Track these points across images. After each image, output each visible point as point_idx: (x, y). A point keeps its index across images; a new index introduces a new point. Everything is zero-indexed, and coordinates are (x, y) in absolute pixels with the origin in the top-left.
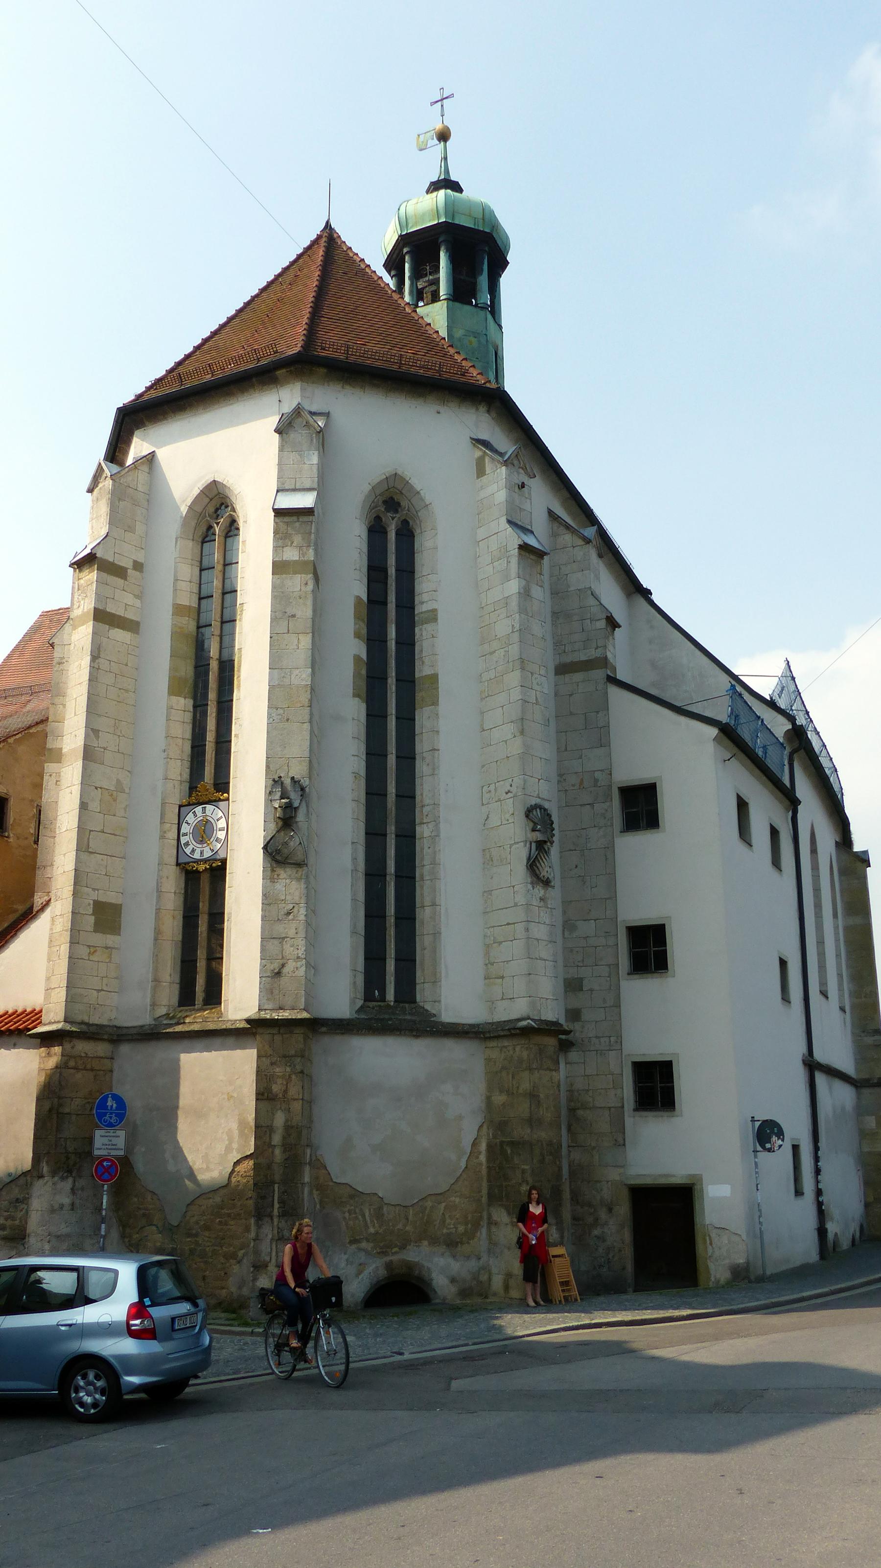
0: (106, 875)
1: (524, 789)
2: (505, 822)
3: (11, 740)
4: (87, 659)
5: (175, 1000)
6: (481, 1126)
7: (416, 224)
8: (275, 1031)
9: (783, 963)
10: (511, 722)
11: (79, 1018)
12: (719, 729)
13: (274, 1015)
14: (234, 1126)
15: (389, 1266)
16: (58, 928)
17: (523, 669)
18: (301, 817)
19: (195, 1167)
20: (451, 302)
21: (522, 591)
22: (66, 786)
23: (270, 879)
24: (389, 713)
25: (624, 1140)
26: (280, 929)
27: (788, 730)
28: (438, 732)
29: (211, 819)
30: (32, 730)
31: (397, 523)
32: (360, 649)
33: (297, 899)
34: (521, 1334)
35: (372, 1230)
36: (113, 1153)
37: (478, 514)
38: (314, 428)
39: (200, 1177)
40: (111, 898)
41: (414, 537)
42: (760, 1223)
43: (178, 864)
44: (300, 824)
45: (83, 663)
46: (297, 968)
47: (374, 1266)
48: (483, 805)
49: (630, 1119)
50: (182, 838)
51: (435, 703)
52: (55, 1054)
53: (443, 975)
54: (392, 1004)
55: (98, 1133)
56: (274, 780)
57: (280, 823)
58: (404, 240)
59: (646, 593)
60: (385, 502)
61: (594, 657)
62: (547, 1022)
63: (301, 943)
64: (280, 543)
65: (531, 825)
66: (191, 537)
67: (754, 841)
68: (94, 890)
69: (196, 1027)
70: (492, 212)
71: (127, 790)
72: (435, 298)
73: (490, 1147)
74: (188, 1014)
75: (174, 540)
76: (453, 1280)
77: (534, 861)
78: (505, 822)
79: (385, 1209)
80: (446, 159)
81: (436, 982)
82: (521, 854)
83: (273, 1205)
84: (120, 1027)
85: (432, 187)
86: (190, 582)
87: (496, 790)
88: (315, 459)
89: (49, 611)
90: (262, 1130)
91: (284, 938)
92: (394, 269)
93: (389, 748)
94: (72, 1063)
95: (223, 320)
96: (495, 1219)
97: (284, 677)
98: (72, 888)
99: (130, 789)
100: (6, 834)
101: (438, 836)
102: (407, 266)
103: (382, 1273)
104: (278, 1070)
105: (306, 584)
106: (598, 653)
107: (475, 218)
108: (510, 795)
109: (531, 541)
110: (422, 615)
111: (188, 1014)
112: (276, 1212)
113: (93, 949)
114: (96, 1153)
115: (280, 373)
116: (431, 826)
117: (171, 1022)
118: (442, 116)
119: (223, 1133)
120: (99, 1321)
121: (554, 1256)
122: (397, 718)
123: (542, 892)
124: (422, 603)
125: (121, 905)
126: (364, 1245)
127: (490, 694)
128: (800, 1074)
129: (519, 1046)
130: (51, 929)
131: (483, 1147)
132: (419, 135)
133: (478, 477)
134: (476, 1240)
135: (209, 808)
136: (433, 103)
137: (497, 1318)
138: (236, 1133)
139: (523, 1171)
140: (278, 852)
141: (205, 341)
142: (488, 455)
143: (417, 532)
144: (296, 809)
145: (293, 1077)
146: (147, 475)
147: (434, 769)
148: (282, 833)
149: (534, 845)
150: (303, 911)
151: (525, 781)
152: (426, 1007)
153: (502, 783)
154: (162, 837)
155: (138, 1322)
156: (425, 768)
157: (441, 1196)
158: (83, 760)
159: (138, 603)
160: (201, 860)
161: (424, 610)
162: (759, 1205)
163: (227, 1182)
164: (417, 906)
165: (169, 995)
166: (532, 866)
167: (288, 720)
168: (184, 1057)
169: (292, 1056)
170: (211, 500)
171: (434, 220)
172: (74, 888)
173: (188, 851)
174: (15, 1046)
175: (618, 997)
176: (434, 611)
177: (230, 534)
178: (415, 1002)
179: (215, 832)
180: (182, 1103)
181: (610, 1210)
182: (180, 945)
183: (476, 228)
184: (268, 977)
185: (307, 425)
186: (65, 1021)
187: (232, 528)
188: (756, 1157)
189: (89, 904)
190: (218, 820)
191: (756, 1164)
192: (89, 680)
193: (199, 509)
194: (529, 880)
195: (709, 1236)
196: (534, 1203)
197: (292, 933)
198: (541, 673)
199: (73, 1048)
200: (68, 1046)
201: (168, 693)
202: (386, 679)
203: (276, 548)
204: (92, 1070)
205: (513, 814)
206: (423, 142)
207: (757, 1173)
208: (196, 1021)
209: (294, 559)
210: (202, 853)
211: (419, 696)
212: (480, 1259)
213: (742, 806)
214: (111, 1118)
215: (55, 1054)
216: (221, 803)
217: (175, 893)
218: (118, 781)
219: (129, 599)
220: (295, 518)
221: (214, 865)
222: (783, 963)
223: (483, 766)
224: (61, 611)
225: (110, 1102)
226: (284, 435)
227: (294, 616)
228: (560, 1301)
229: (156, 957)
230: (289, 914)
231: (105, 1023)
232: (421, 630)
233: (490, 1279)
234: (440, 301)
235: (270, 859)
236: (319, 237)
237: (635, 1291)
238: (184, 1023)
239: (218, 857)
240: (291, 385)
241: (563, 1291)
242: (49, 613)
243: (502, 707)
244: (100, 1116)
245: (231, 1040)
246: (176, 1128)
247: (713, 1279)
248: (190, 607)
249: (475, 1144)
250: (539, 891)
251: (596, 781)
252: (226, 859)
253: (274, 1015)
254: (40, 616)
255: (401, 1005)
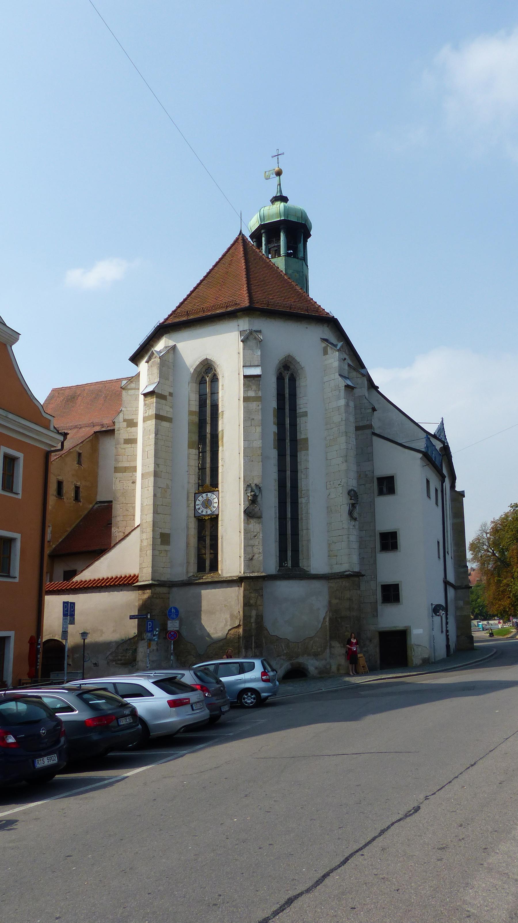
0: (164, 522)
1: (347, 483)
2: (337, 496)
3: (63, 456)
4: (154, 435)
5: (196, 570)
6: (327, 612)
7: (269, 219)
8: (251, 580)
9: (438, 542)
10: (341, 457)
11: (157, 578)
12: (423, 454)
13: (251, 575)
14: (228, 616)
15: (292, 664)
16: (145, 543)
17: (346, 436)
18: (259, 499)
19: (210, 633)
20: (286, 257)
21: (346, 404)
22: (145, 487)
23: (247, 523)
24: (287, 454)
25: (377, 614)
26: (252, 542)
27: (442, 447)
28: (308, 461)
29: (210, 499)
30: (71, 450)
31: (289, 376)
32: (274, 429)
33: (258, 530)
34: (359, 682)
35: (285, 652)
36: (175, 629)
37: (324, 371)
38: (258, 340)
39: (213, 636)
40: (167, 531)
41: (296, 380)
42: (434, 642)
43: (195, 517)
44: (259, 502)
45: (150, 437)
46: (259, 557)
47: (286, 665)
48: (327, 489)
49: (380, 607)
50: (196, 506)
51: (307, 449)
52: (147, 593)
53: (312, 556)
54: (291, 568)
55: (169, 622)
56: (248, 485)
57: (250, 502)
58: (262, 227)
59: (376, 388)
60: (283, 366)
61: (366, 424)
62: (356, 572)
63: (261, 547)
64: (246, 389)
65: (350, 497)
66: (195, 382)
67: (431, 497)
68: (160, 528)
69: (210, 580)
70: (306, 214)
71: (170, 488)
72: (279, 256)
73: (330, 619)
74: (204, 575)
75: (188, 384)
76: (316, 668)
77: (351, 511)
78: (337, 496)
79: (290, 643)
80: (280, 185)
81: (308, 558)
82: (346, 509)
83: (252, 644)
84: (171, 581)
85: (274, 199)
86: (195, 401)
87: (333, 483)
88: (259, 353)
89: (56, 389)
90: (246, 617)
91: (253, 546)
92: (255, 238)
93: (287, 468)
94: (155, 596)
95: (198, 282)
96: (333, 645)
97: (250, 444)
98: (152, 528)
99: (171, 487)
100: (63, 498)
101: (309, 502)
102: (263, 239)
103: (290, 667)
104: (253, 595)
105: (258, 406)
106: (368, 423)
107: (298, 217)
108: (340, 486)
109: (350, 383)
110: (301, 413)
111: (204, 575)
112: (253, 646)
113: (160, 551)
114: (169, 629)
115: (238, 314)
116: (306, 498)
117: (196, 578)
118: (278, 163)
119: (223, 619)
120: (251, 678)
121: (359, 657)
122: (290, 456)
123: (354, 523)
124: (300, 409)
125: (170, 534)
126: (282, 657)
127: (330, 445)
128: (442, 586)
129: (344, 582)
130: (141, 544)
131: (327, 619)
132: (265, 172)
133: (324, 355)
134: (325, 653)
135: (209, 494)
136: (273, 157)
137: (344, 679)
138: (229, 619)
139: (346, 627)
140: (250, 513)
141: (192, 292)
142: (329, 346)
143: (297, 379)
144: (257, 496)
145: (259, 597)
146: (172, 355)
147: (307, 476)
148: (252, 506)
149: (351, 505)
150: (261, 535)
151: (347, 480)
152: (304, 568)
153: (336, 481)
154: (188, 506)
155: (265, 677)
156: (303, 476)
157: (311, 638)
158: (154, 477)
159: (171, 410)
160: (207, 515)
161: (301, 411)
162: (433, 636)
163: (225, 637)
164: (300, 529)
165: (193, 568)
166: (350, 513)
167: (252, 461)
168: (202, 591)
169: (258, 590)
170: (204, 366)
171: (278, 218)
172: (153, 528)
173: (200, 511)
174: (121, 590)
175: (375, 560)
176: (306, 412)
177: (214, 380)
178: (299, 567)
179: (213, 504)
180: (203, 608)
181: (371, 641)
182: (197, 549)
183: (298, 221)
184: (247, 560)
185: (255, 338)
186: (152, 580)
187: (215, 379)
188: (433, 618)
189: (158, 534)
190: (214, 499)
191: (433, 620)
192: (155, 444)
193: (198, 370)
194: (349, 519)
195: (413, 648)
196: (353, 639)
197: (257, 543)
198: (353, 436)
199: (155, 590)
200: (153, 589)
201: (188, 447)
202: (285, 440)
203: (244, 391)
204: (162, 598)
205: (342, 493)
206: (268, 175)
207: (433, 624)
208: (208, 577)
209: (253, 395)
210: (207, 512)
211: (299, 447)
212: (326, 660)
213: (428, 482)
214: (173, 616)
215: (147, 593)
216: (215, 492)
217: (194, 528)
218: (167, 484)
219: (168, 408)
220: (252, 379)
221: (213, 517)
222: (438, 542)
223: (327, 474)
224: (63, 389)
225: (173, 610)
226: (245, 343)
227: (253, 419)
228: (362, 673)
229: (188, 554)
230: (255, 536)
231: (166, 580)
232: (300, 419)
233: (331, 667)
234: (281, 256)
235: (246, 516)
236: (237, 239)
237: (380, 670)
238: (202, 579)
239: (214, 514)
240: (244, 319)
241: (363, 669)
242: (57, 390)
243: (337, 451)
244: (170, 615)
245: (225, 584)
246: (201, 618)
247: (414, 664)
248: (196, 411)
249: (324, 618)
250: (353, 523)
251: (366, 475)
252: (218, 515)
253: (251, 575)
254: (52, 391)
255: (294, 568)
